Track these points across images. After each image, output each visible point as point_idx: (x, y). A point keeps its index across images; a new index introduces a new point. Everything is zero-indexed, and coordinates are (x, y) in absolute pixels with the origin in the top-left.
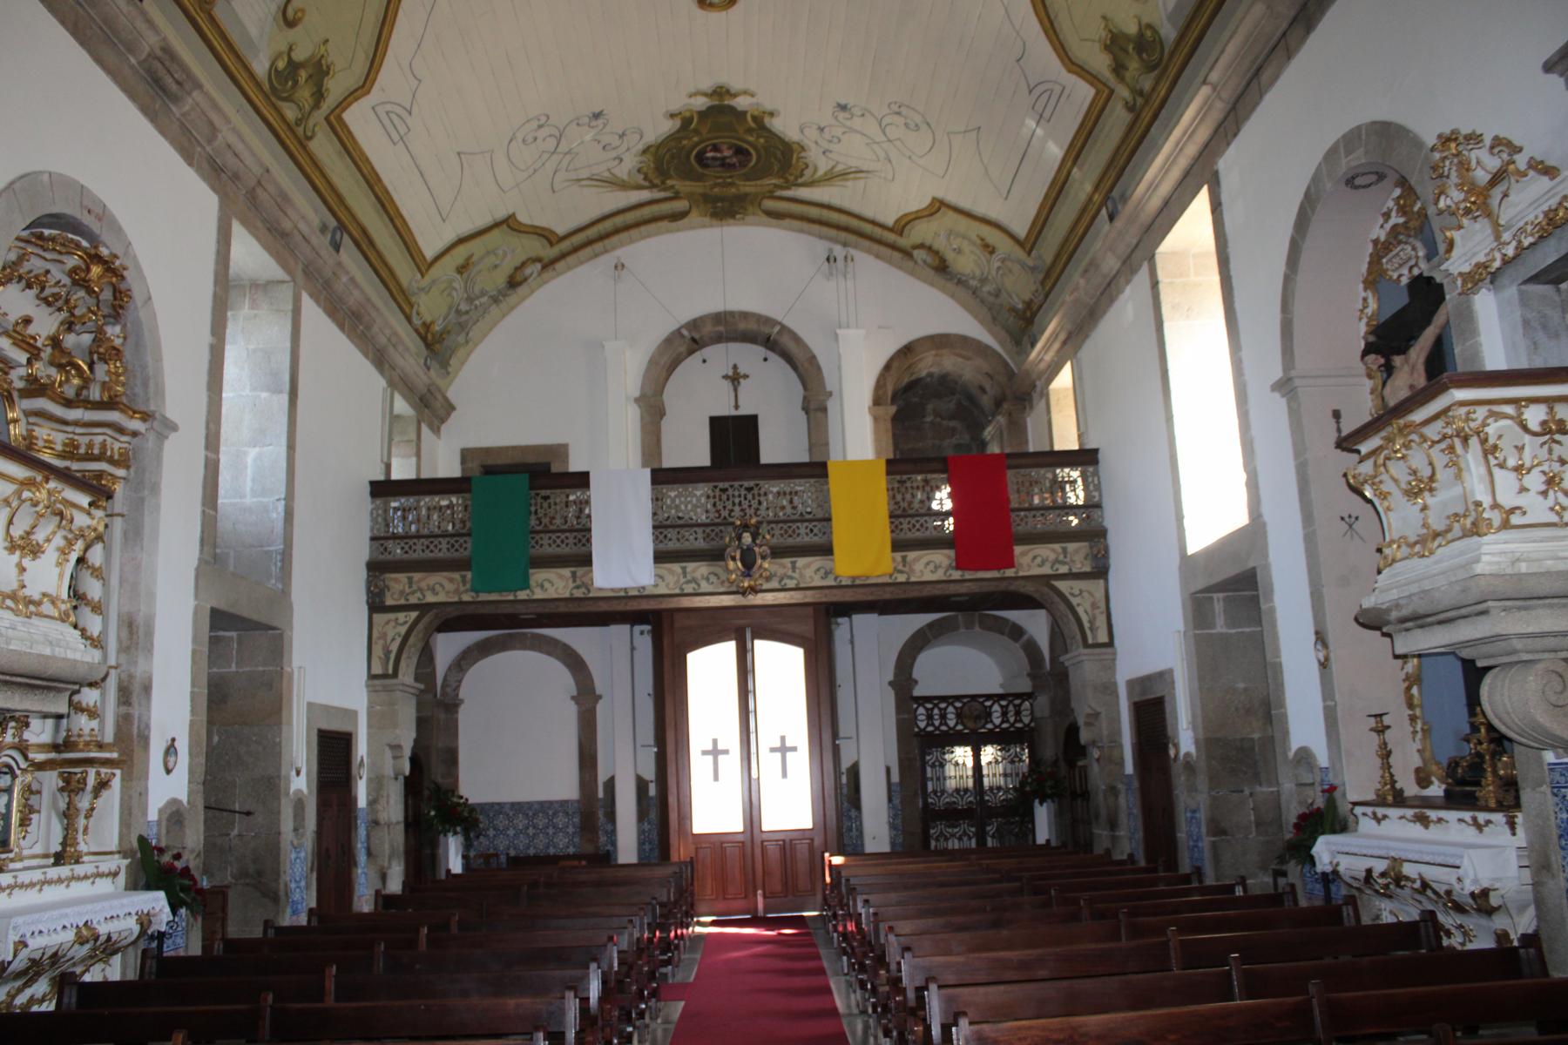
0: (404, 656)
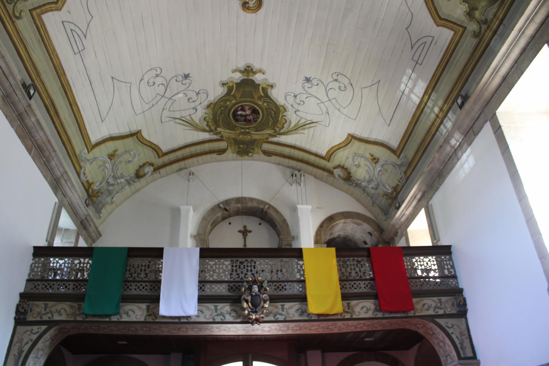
0: (32, 355)
